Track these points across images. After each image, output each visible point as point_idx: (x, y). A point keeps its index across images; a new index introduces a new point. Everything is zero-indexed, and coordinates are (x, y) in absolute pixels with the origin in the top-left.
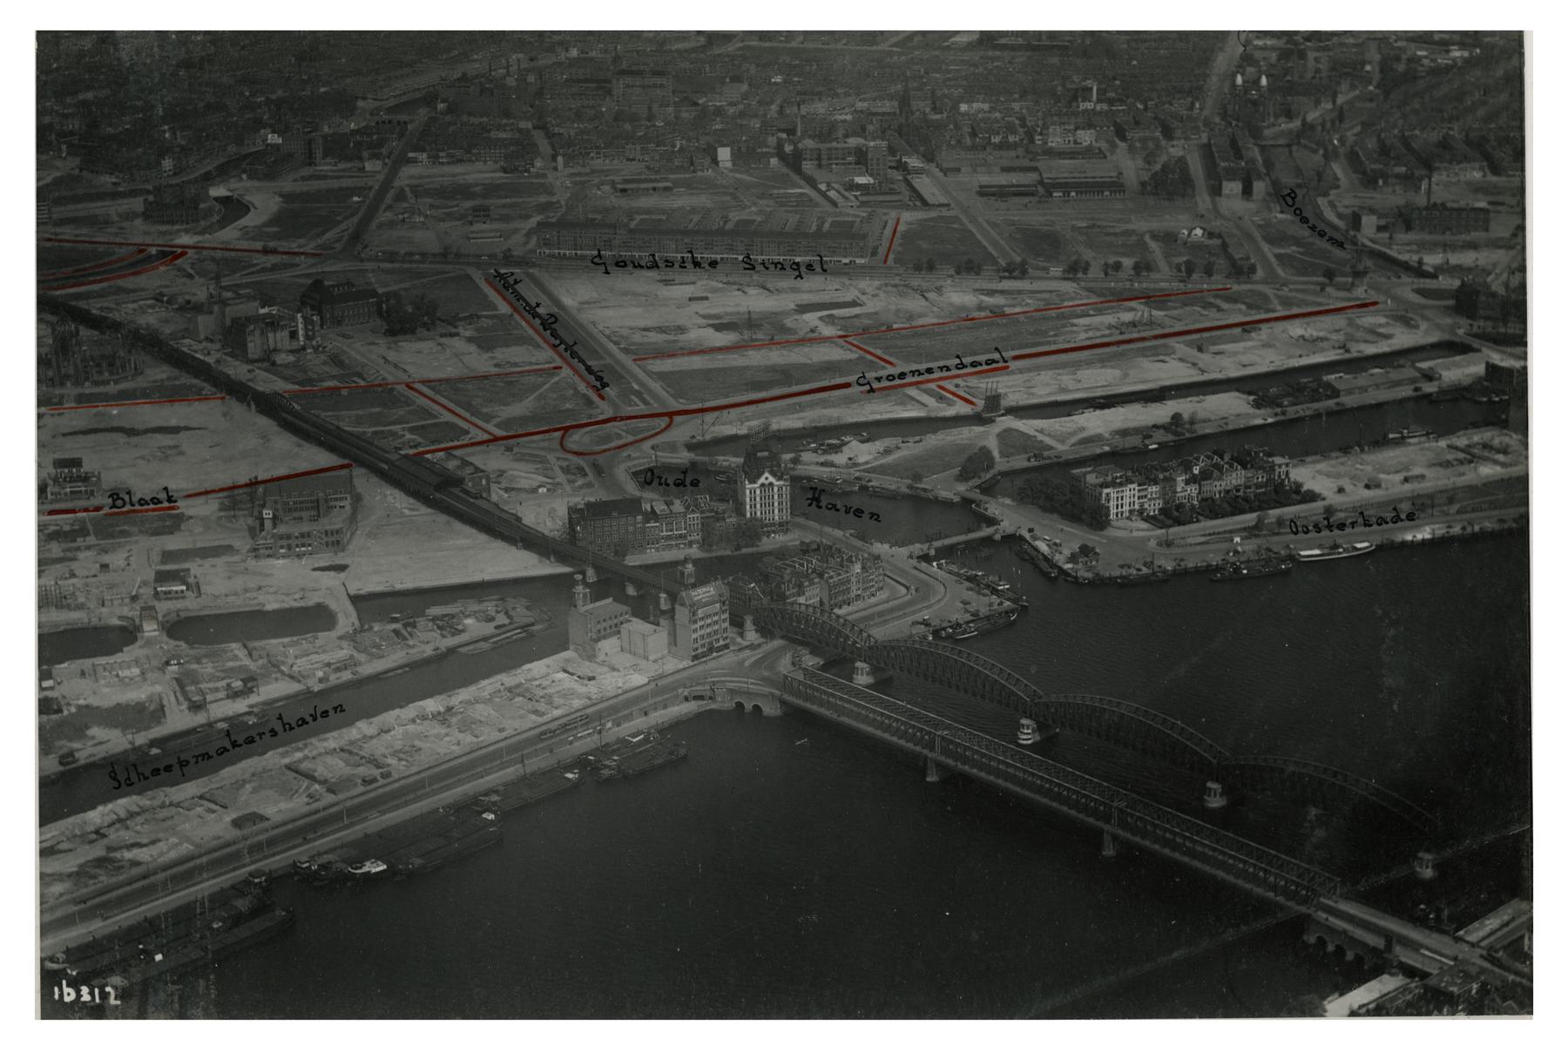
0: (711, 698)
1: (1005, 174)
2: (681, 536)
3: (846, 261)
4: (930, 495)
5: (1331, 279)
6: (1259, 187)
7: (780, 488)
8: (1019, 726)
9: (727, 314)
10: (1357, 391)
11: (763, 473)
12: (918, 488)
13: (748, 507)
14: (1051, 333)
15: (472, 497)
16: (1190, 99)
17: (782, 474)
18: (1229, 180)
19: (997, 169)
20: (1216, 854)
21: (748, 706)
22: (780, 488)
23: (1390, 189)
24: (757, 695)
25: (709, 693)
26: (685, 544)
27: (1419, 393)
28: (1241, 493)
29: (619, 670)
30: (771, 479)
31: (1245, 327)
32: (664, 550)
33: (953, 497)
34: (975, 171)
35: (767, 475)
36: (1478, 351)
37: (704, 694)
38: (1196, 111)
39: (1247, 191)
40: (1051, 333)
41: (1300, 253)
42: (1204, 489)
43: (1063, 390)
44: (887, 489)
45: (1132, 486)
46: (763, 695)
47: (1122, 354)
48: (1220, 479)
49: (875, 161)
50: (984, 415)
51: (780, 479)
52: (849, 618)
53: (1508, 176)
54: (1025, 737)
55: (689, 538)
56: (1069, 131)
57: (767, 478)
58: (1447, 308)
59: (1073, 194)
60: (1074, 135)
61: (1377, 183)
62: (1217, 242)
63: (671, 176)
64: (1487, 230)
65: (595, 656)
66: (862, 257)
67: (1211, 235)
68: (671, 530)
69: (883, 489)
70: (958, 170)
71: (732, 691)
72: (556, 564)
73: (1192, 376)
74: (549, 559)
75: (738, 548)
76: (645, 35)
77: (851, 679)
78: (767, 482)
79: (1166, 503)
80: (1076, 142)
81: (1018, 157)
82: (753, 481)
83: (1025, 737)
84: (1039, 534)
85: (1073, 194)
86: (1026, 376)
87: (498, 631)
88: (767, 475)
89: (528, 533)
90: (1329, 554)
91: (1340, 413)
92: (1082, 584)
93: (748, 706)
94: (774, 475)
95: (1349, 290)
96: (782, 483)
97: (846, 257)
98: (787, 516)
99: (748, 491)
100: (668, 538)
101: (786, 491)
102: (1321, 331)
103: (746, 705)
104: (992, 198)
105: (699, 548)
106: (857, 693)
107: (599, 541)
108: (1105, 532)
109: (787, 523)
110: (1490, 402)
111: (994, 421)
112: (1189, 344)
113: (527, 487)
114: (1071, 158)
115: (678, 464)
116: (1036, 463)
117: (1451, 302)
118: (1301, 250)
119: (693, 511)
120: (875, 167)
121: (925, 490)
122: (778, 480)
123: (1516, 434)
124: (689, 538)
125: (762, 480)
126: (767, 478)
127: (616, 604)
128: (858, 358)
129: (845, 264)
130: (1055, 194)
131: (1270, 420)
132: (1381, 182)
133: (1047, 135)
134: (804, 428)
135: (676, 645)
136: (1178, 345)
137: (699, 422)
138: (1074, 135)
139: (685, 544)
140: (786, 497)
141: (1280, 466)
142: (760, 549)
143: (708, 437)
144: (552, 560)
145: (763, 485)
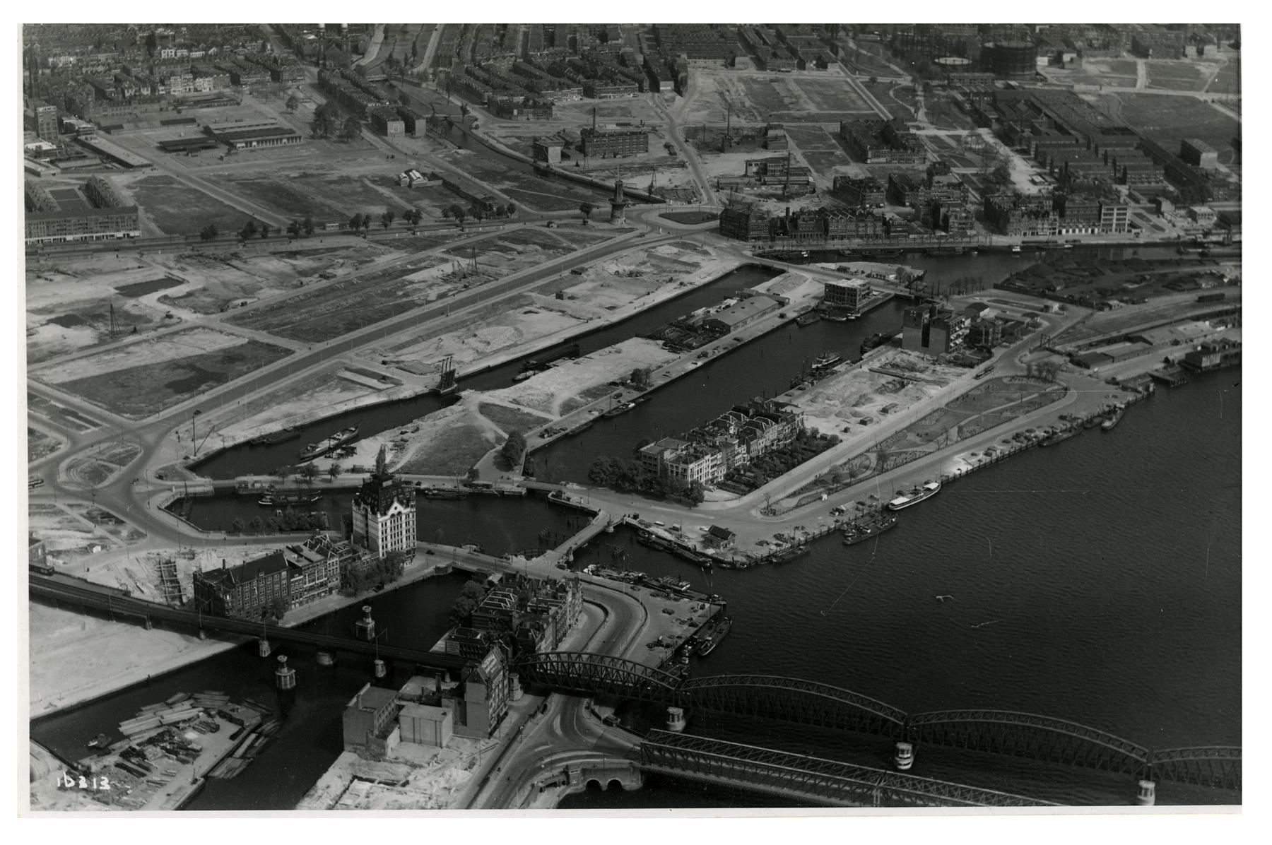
0: (563, 783)
1: (166, 128)
2: (322, 585)
3: (120, 234)
4: (493, 490)
5: (588, 213)
6: (420, 125)
7: (407, 516)
8: (897, 752)
9: (61, 305)
10: (741, 324)
12: (478, 485)
13: (380, 541)
14: (400, 293)
15: (44, 574)
16: (260, 42)
17: (408, 501)
18: (393, 120)
19: (157, 123)
21: (604, 783)
22: (407, 516)
23: (524, 118)
25: (563, 778)
26: (325, 592)
27: (785, 320)
28: (775, 447)
29: (421, 767)
30: (400, 508)
32: (307, 602)
33: (519, 490)
34: (137, 127)
35: (396, 504)
36: (783, 272)
37: (556, 780)
38: (268, 52)
39: (410, 129)
40: (400, 293)
41: (518, 187)
43: (482, 355)
44: (444, 490)
46: (621, 770)
48: (762, 437)
49: (45, 126)
50: (442, 392)
51: (407, 506)
52: (589, 650)
53: (600, 98)
54: (906, 762)
55: (329, 585)
56: (189, 80)
57: (396, 507)
58: (712, 231)
61: (512, 113)
63: (785, 124)
65: (384, 754)
66: (135, 229)
67: (433, 176)
68: (314, 580)
69: (438, 490)
70: (120, 127)
71: (584, 771)
72: (208, 641)
73: (572, 329)
74: (199, 637)
77: (666, 727)
79: (728, 468)
80: (196, 90)
81: (161, 109)
83: (906, 762)
85: (254, 144)
86: (435, 340)
87: (236, 742)
88: (396, 504)
89: (154, 609)
90: (914, 500)
91: (741, 348)
92: (740, 570)
93: (604, 783)
95: (609, 221)
97: (118, 231)
99: (380, 525)
100: (312, 588)
101: (412, 518)
102: (630, 265)
103: (601, 783)
104: (181, 153)
105: (338, 593)
106: (675, 740)
107: (247, 607)
109: (414, 550)
111: (459, 398)
113: (73, 547)
114: (208, 107)
115: (204, 493)
116: (551, 439)
117: (716, 223)
118: (516, 184)
119: (332, 556)
120: (46, 131)
121: (487, 486)
123: (914, 351)
124: (329, 585)
125: (392, 511)
126: (396, 507)
127: (375, 689)
129: (120, 238)
130: (238, 145)
135: (465, 724)
139: (325, 592)
140: (412, 526)
141: (798, 415)
142: (404, 580)
143: (201, 456)
144: (202, 636)
145: (393, 516)
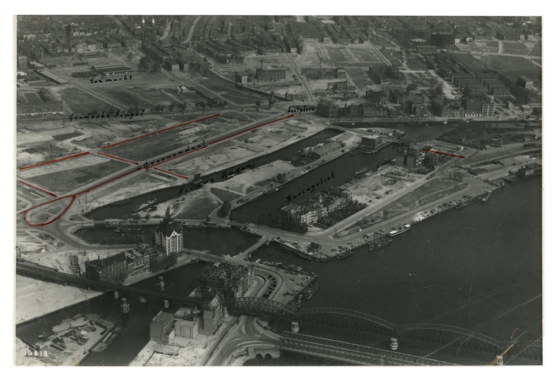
2: (142, 267)
6: (186, 66)
7: (179, 237)
8: (391, 342)
10: (325, 154)
11: (173, 231)
12: (210, 224)
13: (167, 248)
16: (116, 29)
18: (174, 64)
19: (71, 65)
20: (336, 351)
22: (179, 237)
23: (231, 64)
24: (268, 349)
26: (143, 270)
27: (344, 153)
28: (339, 208)
29: (184, 347)
30: (176, 234)
31: (253, 130)
32: (135, 275)
35: (174, 232)
39: (182, 68)
40: (177, 140)
42: (329, 209)
44: (195, 226)
45: (309, 213)
47: (217, 147)
48: (334, 204)
49: (22, 65)
51: (179, 233)
53: (265, 55)
54: (395, 346)
57: (174, 233)
59: (114, 74)
60: (87, 47)
61: (226, 61)
62: (194, 91)
64: (285, 78)
65: (168, 342)
66: (61, 111)
67: (191, 89)
68: (138, 265)
70: (55, 66)
72: (91, 291)
74: (87, 289)
75: (167, 268)
76: (105, 17)
77: (290, 330)
78: (174, 235)
80: (88, 50)
82: (169, 236)
83: (395, 346)
84: (283, 240)
87: (103, 336)
88: (174, 232)
93: (263, 355)
94: (177, 232)
95: (268, 109)
96: (180, 234)
97: (54, 111)
98: (182, 249)
99: (167, 241)
100: (137, 269)
103: (263, 355)
105: (148, 271)
106: (294, 336)
108: (308, 234)
110: (372, 153)
112: (239, 139)
114: (93, 58)
116: (241, 204)
119: (146, 255)
120: (22, 67)
122: (178, 234)
123: (400, 167)
125: (172, 235)
126: (174, 233)
128: (110, 161)
131: (307, 172)
132: (228, 61)
133: (77, 48)
134: (126, 199)
136: (235, 141)
137: (78, 202)
138: (87, 47)
139: (143, 270)
143: (89, 210)
144: (89, 289)
145: (173, 237)
